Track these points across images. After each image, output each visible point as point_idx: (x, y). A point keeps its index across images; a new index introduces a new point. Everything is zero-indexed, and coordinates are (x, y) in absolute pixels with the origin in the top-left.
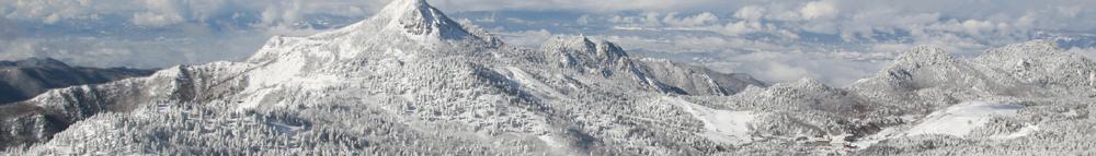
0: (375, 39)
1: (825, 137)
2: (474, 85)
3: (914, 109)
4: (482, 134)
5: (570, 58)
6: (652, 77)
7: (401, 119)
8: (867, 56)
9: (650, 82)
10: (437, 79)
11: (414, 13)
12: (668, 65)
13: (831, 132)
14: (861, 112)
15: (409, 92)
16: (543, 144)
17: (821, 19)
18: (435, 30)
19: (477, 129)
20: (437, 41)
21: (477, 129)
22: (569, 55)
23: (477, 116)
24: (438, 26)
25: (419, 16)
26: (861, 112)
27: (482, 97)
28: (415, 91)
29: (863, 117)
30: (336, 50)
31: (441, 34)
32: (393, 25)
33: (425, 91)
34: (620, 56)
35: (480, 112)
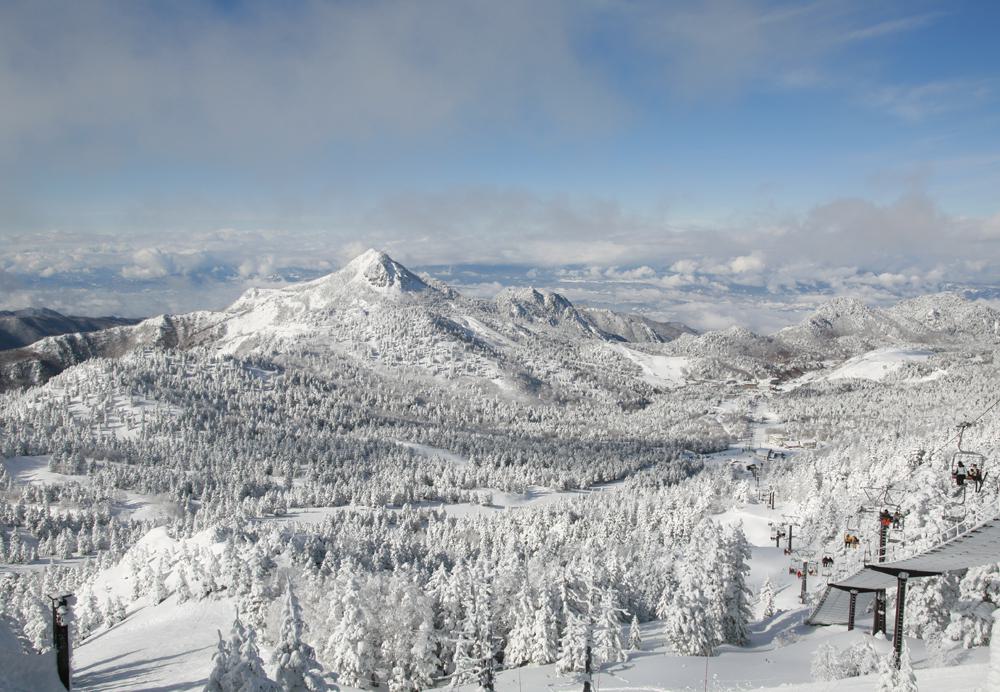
0: (342, 290)
1: (753, 380)
2: (432, 333)
3: (834, 355)
4: (439, 378)
6: (595, 326)
9: (593, 330)
10: (398, 327)
11: (378, 267)
15: (373, 339)
18: (397, 283)
20: (399, 293)
23: (435, 361)
24: (400, 279)
25: (383, 270)
27: (440, 344)
29: (787, 363)
31: (403, 287)
32: (359, 278)
33: (388, 338)
35: (438, 358)
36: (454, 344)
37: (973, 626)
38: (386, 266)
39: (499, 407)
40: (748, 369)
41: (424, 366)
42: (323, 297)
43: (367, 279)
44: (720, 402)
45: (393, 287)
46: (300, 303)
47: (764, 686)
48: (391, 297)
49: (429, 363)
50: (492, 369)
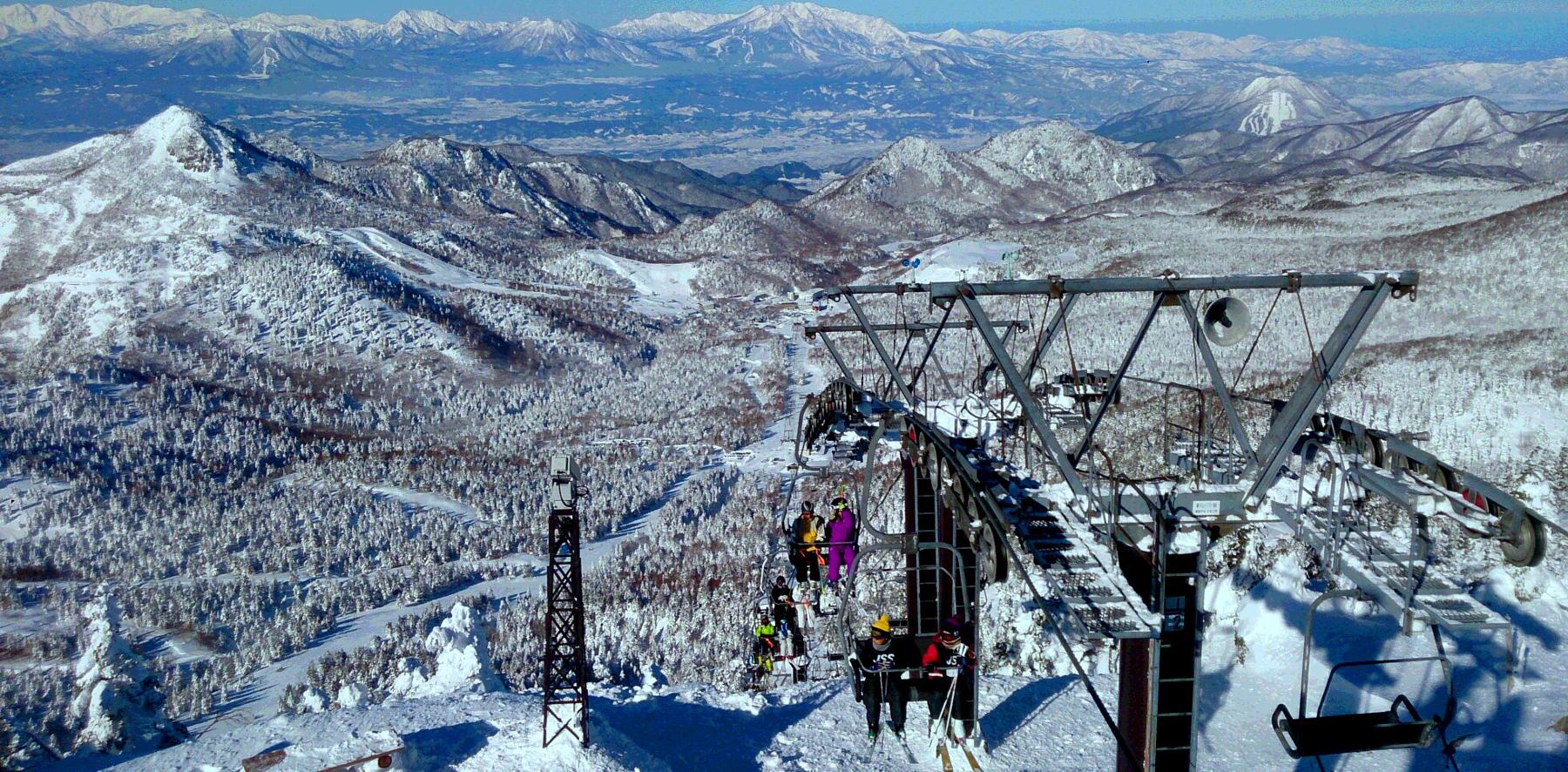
0: (131, 182)
1: (790, 295)
2: (344, 290)
3: (900, 232)
4: (367, 356)
5: (429, 179)
6: (550, 196)
7: (255, 350)
8: (844, 116)
9: (548, 203)
10: (291, 283)
11: (192, 139)
12: (568, 171)
13: (797, 283)
14: (834, 243)
15: (255, 306)
16: (449, 360)
17: (1441, 674)
18: (229, 164)
19: (361, 350)
20: (235, 180)
21: (361, 350)
22: (424, 173)
23: (357, 332)
24: (231, 156)
25: (201, 144)
26: (834, 243)
27: (357, 305)
28: (264, 304)
29: (836, 253)
30: (67, 203)
31: (239, 169)
32: (159, 156)
33: (277, 302)
34: (500, 169)
35: (360, 325)
36: (377, 302)
37: (1422, 521)
38: (206, 137)
39: (461, 393)
40: (783, 275)
41: (341, 340)
42: (99, 192)
43: (175, 158)
44: (748, 349)
45: (222, 172)
46: (57, 205)
47: (387, 42)
48: (223, 189)
49: (347, 336)
50: (437, 336)
